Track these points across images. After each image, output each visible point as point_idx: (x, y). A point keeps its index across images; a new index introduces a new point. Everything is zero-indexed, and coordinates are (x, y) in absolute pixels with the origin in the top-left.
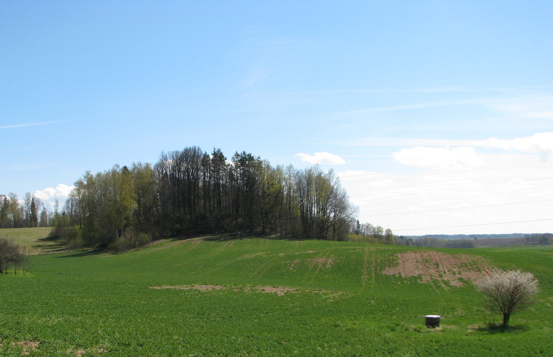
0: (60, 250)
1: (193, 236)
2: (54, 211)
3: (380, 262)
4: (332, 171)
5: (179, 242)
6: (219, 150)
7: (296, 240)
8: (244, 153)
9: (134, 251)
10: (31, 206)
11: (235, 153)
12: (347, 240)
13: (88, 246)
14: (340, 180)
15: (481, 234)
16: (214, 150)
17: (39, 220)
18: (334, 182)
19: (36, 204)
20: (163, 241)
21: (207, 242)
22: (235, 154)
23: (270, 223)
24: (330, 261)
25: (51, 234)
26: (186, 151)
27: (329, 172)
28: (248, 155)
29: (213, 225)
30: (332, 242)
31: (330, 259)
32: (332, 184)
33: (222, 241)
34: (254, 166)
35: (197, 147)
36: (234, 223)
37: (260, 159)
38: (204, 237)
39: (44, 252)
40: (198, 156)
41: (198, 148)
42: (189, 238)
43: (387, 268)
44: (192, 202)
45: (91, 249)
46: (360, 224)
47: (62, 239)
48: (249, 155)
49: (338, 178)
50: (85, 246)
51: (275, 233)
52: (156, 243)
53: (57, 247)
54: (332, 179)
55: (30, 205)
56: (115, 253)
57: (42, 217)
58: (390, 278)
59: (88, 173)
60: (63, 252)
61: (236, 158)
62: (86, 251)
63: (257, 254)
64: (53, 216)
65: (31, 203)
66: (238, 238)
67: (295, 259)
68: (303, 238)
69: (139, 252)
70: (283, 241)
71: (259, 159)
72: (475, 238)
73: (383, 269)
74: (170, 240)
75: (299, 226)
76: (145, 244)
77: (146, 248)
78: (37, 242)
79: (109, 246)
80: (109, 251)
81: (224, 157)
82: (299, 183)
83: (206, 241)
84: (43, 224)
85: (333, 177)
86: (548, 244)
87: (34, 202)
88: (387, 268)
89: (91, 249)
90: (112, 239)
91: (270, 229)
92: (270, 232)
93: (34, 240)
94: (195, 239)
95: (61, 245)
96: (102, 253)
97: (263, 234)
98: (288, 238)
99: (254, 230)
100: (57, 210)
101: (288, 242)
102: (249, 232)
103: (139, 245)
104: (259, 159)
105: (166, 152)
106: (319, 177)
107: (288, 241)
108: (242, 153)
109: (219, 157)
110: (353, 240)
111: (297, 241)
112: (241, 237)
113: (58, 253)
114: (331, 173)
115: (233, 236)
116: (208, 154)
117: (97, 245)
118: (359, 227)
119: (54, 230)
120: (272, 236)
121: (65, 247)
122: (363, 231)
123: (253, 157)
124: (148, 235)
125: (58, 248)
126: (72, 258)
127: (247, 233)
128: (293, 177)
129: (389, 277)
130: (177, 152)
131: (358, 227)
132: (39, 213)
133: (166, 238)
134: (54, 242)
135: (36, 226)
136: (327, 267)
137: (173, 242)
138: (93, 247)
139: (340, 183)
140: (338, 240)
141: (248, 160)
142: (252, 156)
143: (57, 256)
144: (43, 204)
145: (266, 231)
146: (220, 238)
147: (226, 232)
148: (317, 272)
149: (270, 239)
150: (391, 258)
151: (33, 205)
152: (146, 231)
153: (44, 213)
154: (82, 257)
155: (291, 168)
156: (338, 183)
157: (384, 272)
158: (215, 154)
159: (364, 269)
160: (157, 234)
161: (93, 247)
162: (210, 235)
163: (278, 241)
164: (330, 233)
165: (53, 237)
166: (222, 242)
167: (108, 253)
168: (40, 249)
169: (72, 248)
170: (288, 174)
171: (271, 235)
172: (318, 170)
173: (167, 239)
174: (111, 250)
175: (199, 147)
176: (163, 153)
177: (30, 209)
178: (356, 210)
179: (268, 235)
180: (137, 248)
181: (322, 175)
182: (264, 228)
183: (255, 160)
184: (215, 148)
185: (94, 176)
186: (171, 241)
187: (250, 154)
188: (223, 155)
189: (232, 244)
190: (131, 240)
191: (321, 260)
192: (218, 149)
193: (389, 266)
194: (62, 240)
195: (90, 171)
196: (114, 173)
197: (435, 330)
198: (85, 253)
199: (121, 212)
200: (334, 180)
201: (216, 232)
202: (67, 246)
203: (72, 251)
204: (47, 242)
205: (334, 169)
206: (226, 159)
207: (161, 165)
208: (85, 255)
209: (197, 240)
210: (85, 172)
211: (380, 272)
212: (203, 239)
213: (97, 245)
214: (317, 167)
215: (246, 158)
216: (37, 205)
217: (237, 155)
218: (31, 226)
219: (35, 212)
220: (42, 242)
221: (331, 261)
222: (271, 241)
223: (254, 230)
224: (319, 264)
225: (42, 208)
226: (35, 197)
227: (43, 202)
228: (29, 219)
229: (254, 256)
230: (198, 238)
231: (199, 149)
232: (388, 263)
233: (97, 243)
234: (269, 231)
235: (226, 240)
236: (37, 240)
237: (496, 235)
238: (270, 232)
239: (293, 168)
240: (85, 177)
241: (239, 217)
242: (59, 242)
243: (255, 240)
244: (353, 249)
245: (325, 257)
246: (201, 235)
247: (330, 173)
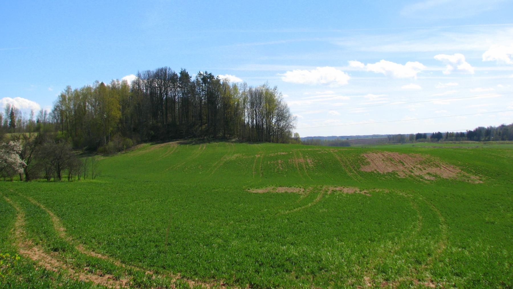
4: (276, 88)
8: (206, 72)
10: (10, 115)
11: (199, 72)
15: (349, 136)
19: (15, 113)
22: (198, 73)
28: (209, 74)
35: (168, 67)
37: (219, 77)
38: (178, 142)
41: (169, 68)
48: (210, 74)
49: (280, 93)
54: (276, 94)
65: (10, 112)
72: (347, 139)
86: (405, 142)
92: (230, 137)
94: (171, 143)
102: (213, 137)
104: (218, 78)
108: (204, 72)
109: (185, 75)
115: (203, 141)
116: (176, 73)
130: (148, 71)
133: (145, 142)
147: (195, 136)
158: (182, 73)
160: (139, 140)
162: (183, 139)
175: (170, 67)
182: (224, 134)
195: (70, 86)
206: (191, 77)
209: (173, 144)
212: (178, 143)
216: (16, 114)
226: (14, 107)
230: (173, 142)
231: (170, 69)
235: (196, 143)
237: (376, 135)
238: (230, 137)
240: (66, 91)
247: (275, 88)
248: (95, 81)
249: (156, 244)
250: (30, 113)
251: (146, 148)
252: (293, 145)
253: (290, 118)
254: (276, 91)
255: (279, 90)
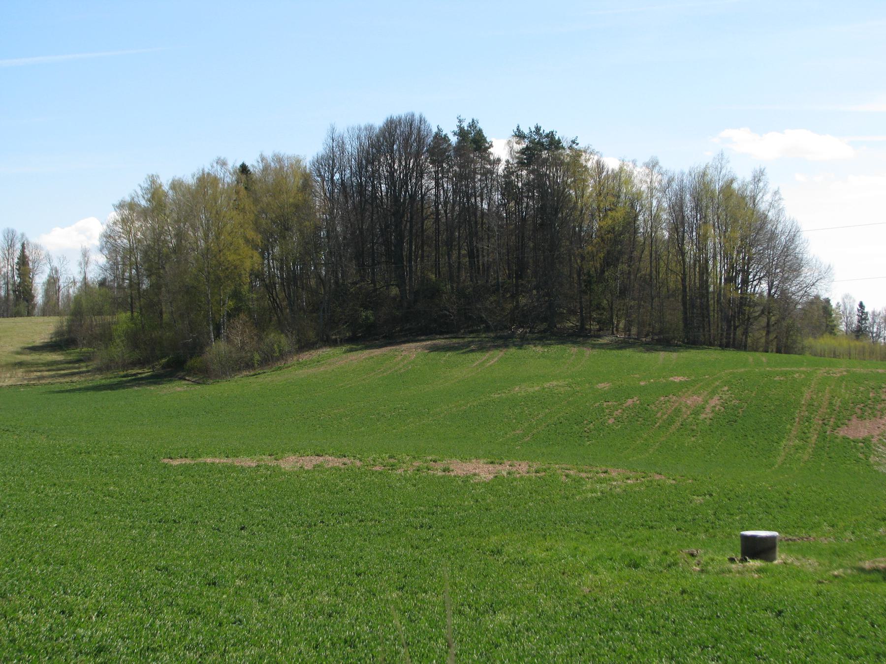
0: (73, 374)
1: (403, 339)
2: (79, 278)
3: (840, 406)
5: (366, 353)
6: (473, 125)
7: (662, 351)
8: (538, 129)
9: (247, 376)
10: (18, 263)
11: (515, 130)
12: (801, 352)
13: (141, 363)
14: (782, 197)
16: (459, 124)
17: (39, 298)
18: (767, 204)
19: (31, 258)
20: (325, 352)
21: (432, 355)
23: (599, 307)
24: (715, 401)
25: (58, 333)
26: (391, 126)
27: (755, 177)
28: (547, 136)
29: (453, 313)
30: (763, 357)
31: (716, 397)
32: (763, 206)
33: (472, 351)
34: (557, 162)
35: (417, 117)
36: (509, 306)
37: (577, 144)
38: (429, 342)
39: (30, 380)
40: (420, 140)
42: (391, 344)
43: (854, 420)
44: (404, 254)
45: (146, 372)
46: (866, 311)
47: (84, 345)
48: (551, 136)
49: (776, 193)
50: (134, 364)
51: (613, 333)
52: (305, 356)
53: (66, 365)
54: (761, 195)
55: (16, 260)
56: (201, 381)
57: (47, 292)
58: (855, 445)
59: (153, 180)
60: (75, 379)
61: (518, 143)
62: (134, 377)
63: (546, 385)
64: (73, 291)
65: (17, 254)
66: (515, 345)
67: (629, 396)
68: (680, 346)
69: (261, 379)
70: (628, 352)
71: (574, 145)
73: (843, 424)
74: (344, 348)
75: (674, 316)
76: (278, 359)
77: (280, 368)
78: (18, 353)
79: (190, 363)
80: (189, 376)
81: (486, 142)
82: (677, 208)
83: (432, 353)
84: (50, 309)
85: (763, 191)
87: (27, 253)
88: (854, 420)
89: (147, 371)
90: (197, 348)
91: (599, 322)
92: (600, 330)
93: (12, 349)
95: (79, 361)
96: (170, 381)
97: (580, 336)
98: (643, 344)
99: (558, 326)
100: (85, 273)
101: (640, 354)
102: (545, 331)
103: (262, 362)
104: (574, 145)
105: (341, 129)
106: (727, 189)
107: (640, 351)
108: (533, 129)
110: (834, 354)
111: (662, 353)
112: (523, 342)
113: (65, 380)
114: (759, 180)
115: (504, 341)
116: (444, 133)
117: (164, 360)
118: (866, 319)
119: (65, 324)
120: (601, 341)
121: (87, 366)
122: (875, 330)
123: (559, 142)
124: (287, 336)
125: (70, 368)
126: (90, 393)
127: (540, 332)
128: (660, 191)
129: (852, 443)
130: (370, 128)
131: (863, 319)
132: (39, 282)
133: (334, 343)
134: (62, 354)
135: (29, 314)
136: (702, 416)
137: (352, 353)
138: (153, 367)
139: (783, 204)
140: (778, 351)
141: (546, 149)
142: (557, 138)
143: (57, 389)
144: (49, 258)
145: (588, 327)
146: (468, 344)
147: (488, 329)
148: (672, 429)
149: (594, 347)
150: (871, 395)
151: (23, 260)
152: (281, 327)
153: (52, 282)
154: (100, 393)
155: (654, 166)
156: (776, 205)
157: (841, 433)
158: (462, 134)
159: (795, 424)
160: (311, 335)
161: (153, 367)
162: (445, 336)
163: (615, 352)
164: (757, 333)
165: (57, 344)
166: (471, 356)
167: (184, 382)
168: (20, 372)
169: (99, 370)
170: (647, 182)
171: (599, 337)
172: (723, 172)
173: (338, 346)
174: (195, 374)
176: (333, 130)
177: (16, 272)
178: (825, 274)
179: (591, 336)
180: (257, 370)
181: (735, 186)
183: (563, 148)
184: (461, 118)
185: (166, 187)
186: (345, 352)
187: (552, 132)
188: (483, 136)
189: (496, 359)
190: (242, 348)
191: (692, 400)
192: (471, 121)
193: (861, 417)
194: (84, 349)
196: (206, 181)
197: (744, 567)
198: (129, 381)
199: (218, 278)
200: (768, 198)
201: (462, 331)
202: (93, 365)
203: (98, 377)
204: (44, 354)
205: (765, 171)
207: (329, 162)
208: (128, 387)
210: (146, 176)
211: (833, 429)
212: (426, 348)
213: (164, 360)
214: (719, 165)
215: (542, 144)
216: (34, 262)
217: (520, 135)
218: (18, 314)
219: (27, 279)
220: (30, 354)
221: (717, 402)
222: (595, 352)
223: (558, 326)
224: (684, 410)
225: (47, 271)
227: (50, 254)
228: (12, 297)
229: (537, 389)
232: (861, 409)
233: (164, 357)
234: (598, 327)
235: (482, 348)
236: (19, 350)
238: (600, 330)
239: (661, 168)
241: (522, 291)
242: (73, 354)
243: (555, 349)
244: (785, 374)
245: (706, 393)
246: (423, 337)
248: (215, 158)
249: (858, 343)
250: (79, 257)
251: (323, 362)
252: (321, 458)
253: (797, 239)
254: (761, 184)
255: (772, 182)
